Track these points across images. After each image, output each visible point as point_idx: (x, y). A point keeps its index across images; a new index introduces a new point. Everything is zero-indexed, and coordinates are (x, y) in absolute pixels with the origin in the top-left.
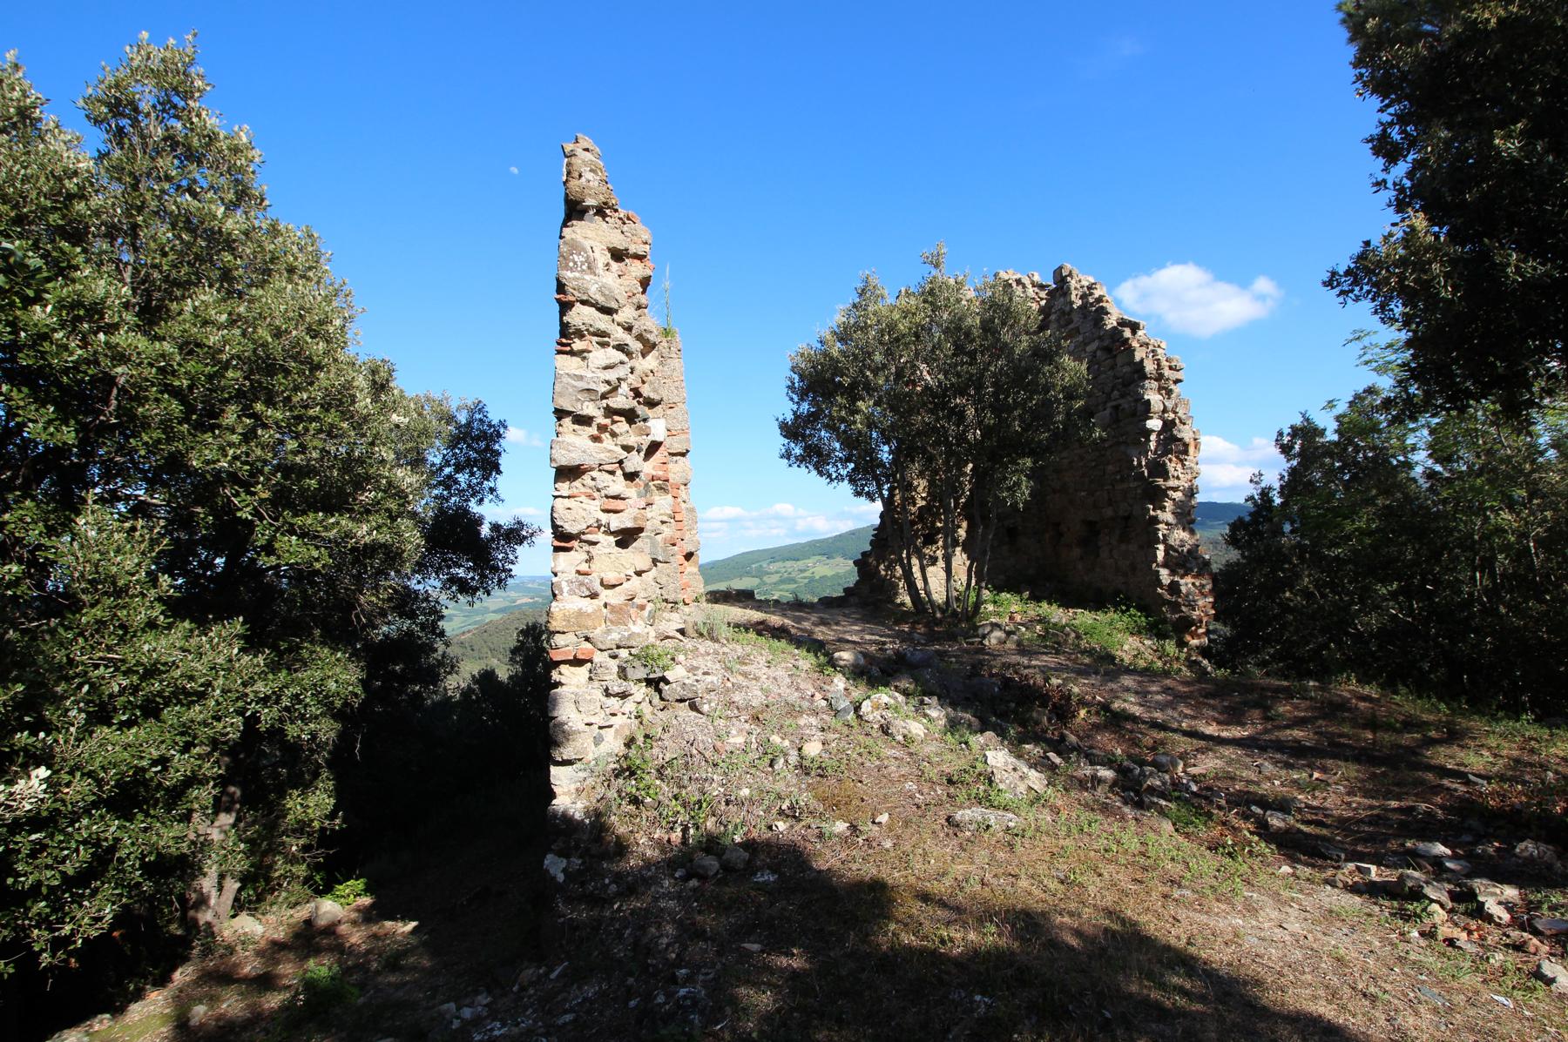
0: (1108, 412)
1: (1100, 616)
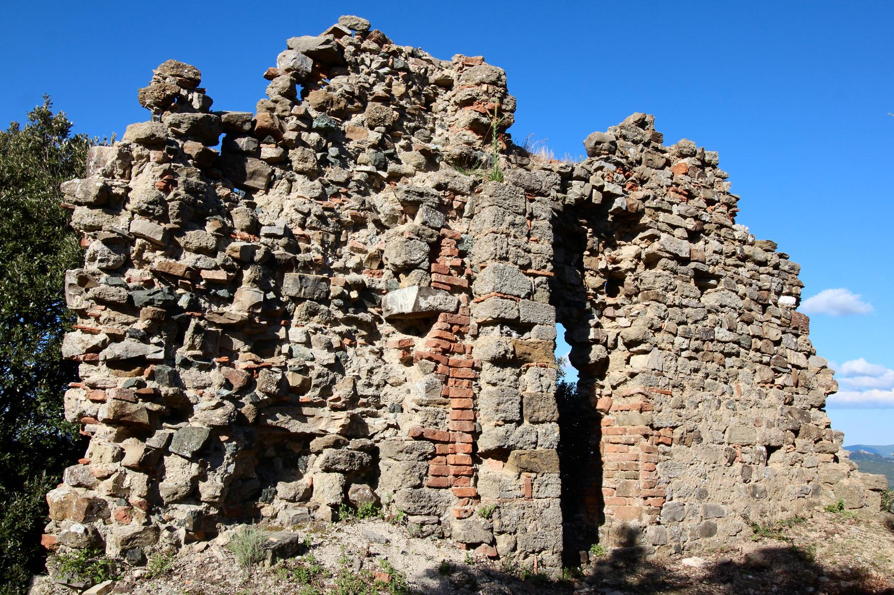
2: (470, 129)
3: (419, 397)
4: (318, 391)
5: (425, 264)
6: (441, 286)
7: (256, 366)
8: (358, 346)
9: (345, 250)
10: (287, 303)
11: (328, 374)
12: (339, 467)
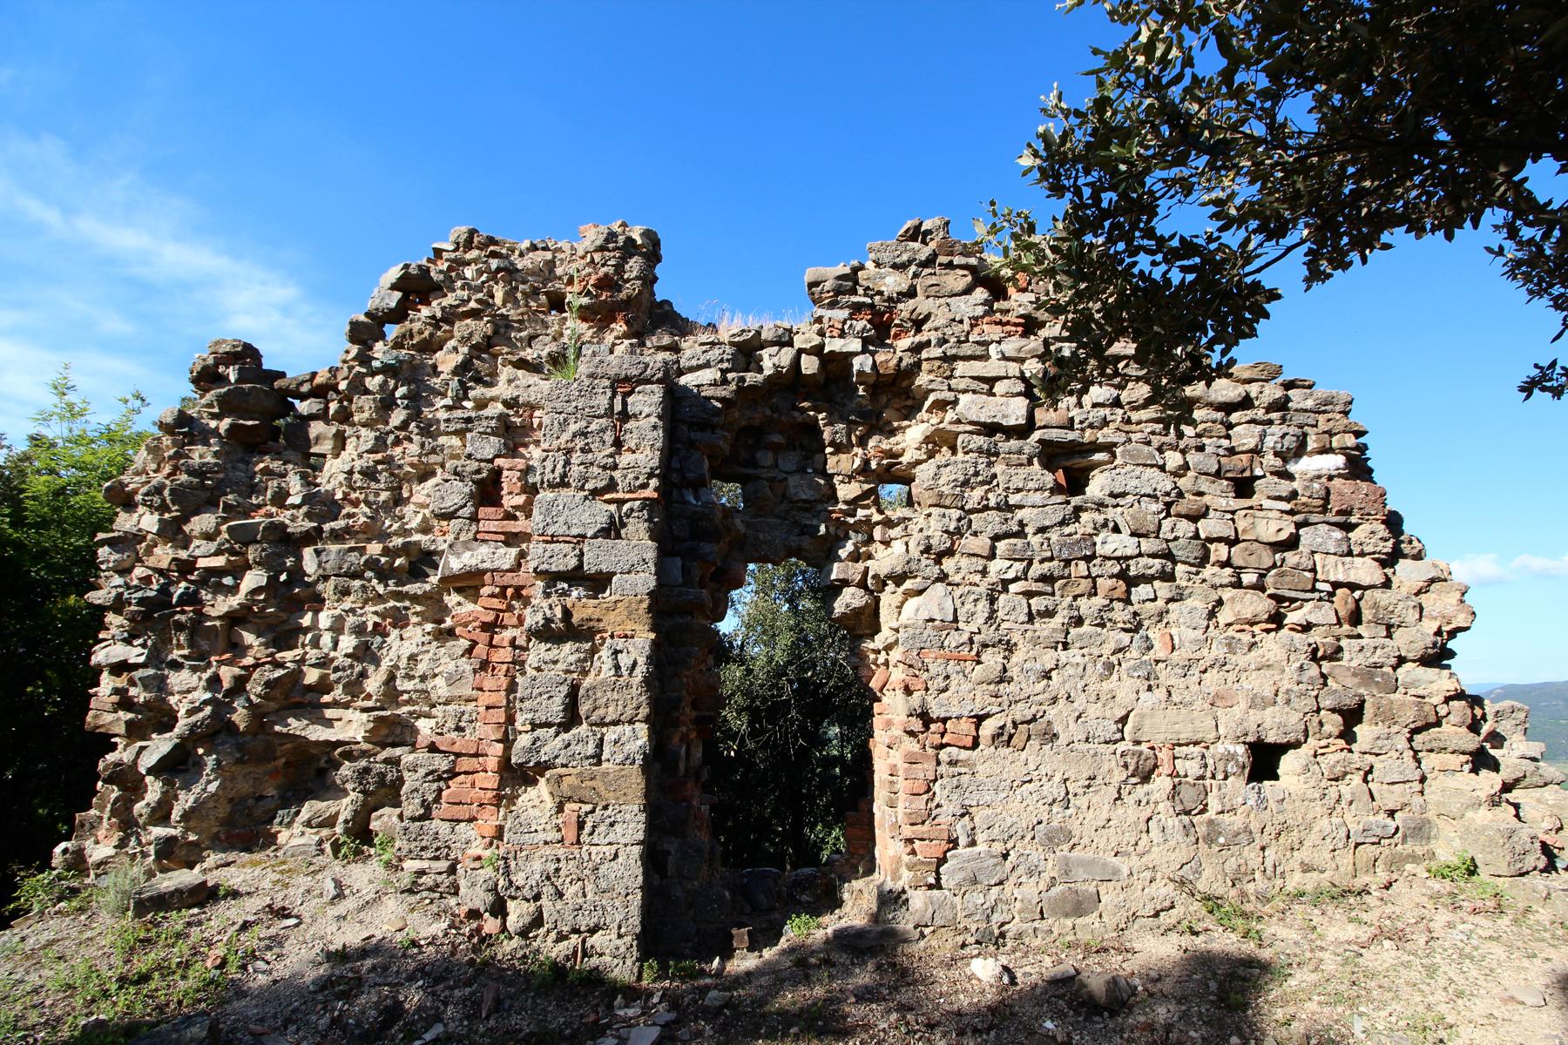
5: (466, 512)
9: (408, 510)
11: (351, 666)
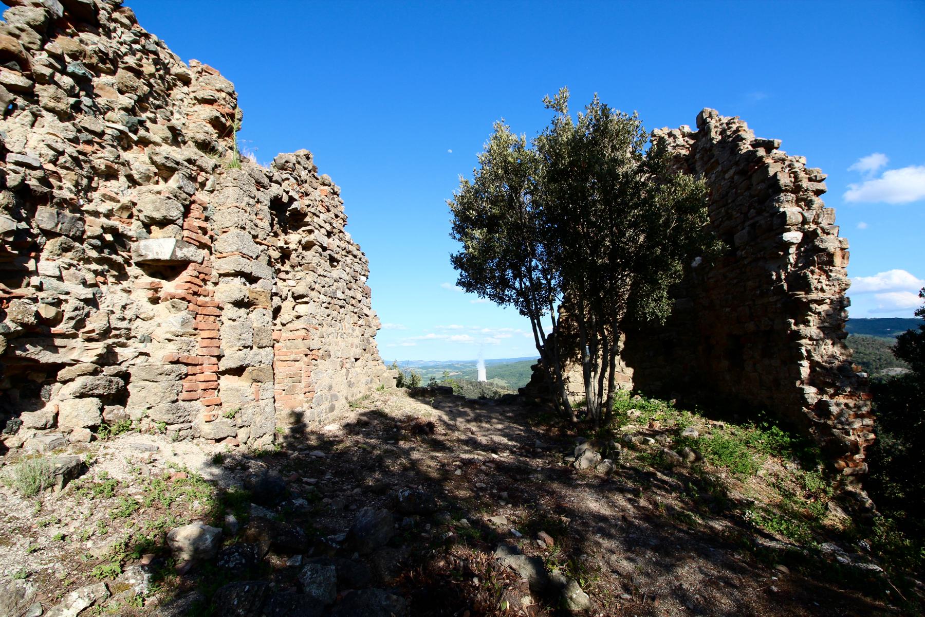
0: (747, 229)
1: (740, 432)
2: (210, 123)
3: (173, 329)
4: (73, 323)
6: (192, 241)
7: (8, 296)
8: (110, 284)
9: (95, 195)
10: (37, 236)
12: (96, 392)
